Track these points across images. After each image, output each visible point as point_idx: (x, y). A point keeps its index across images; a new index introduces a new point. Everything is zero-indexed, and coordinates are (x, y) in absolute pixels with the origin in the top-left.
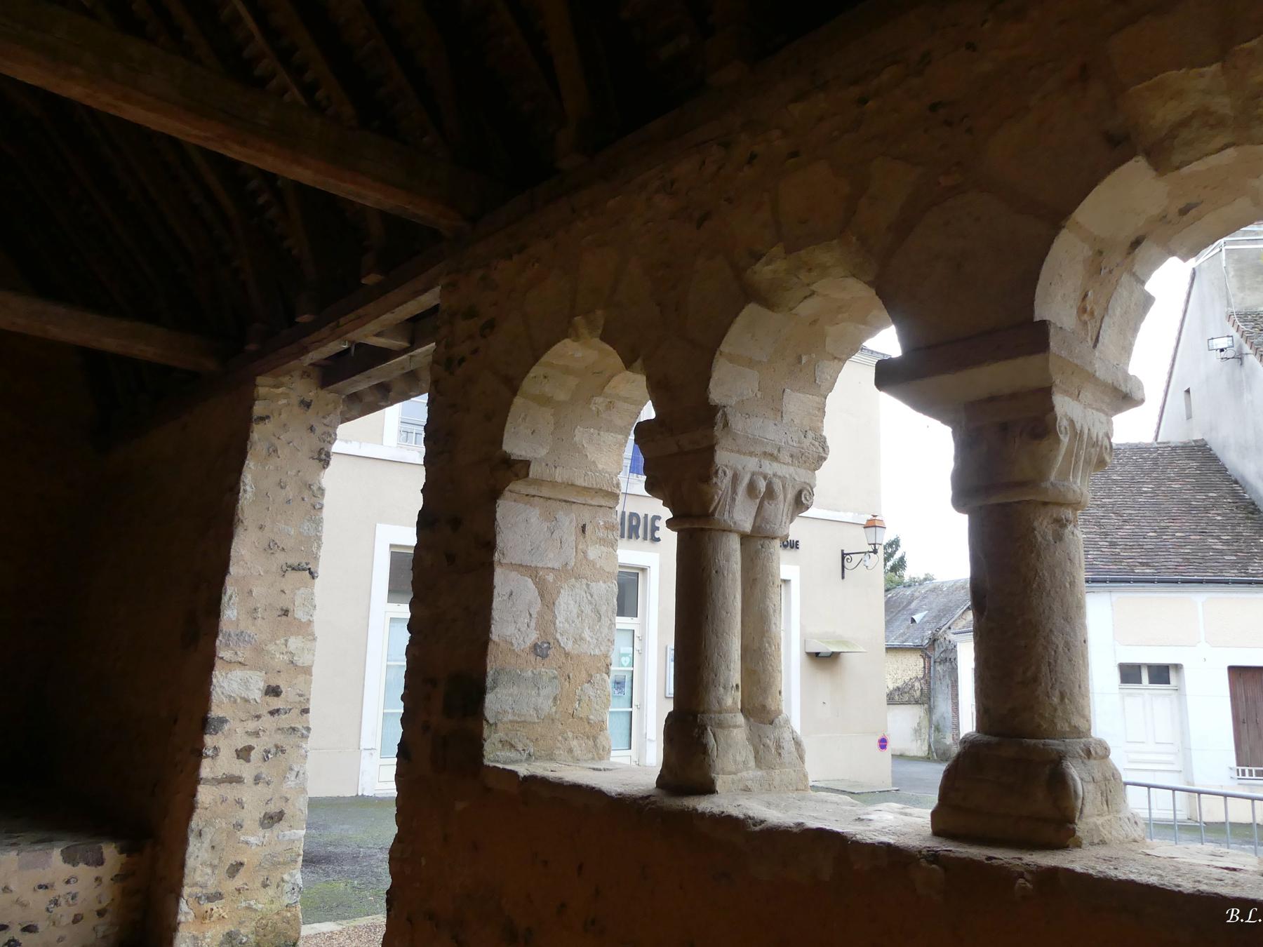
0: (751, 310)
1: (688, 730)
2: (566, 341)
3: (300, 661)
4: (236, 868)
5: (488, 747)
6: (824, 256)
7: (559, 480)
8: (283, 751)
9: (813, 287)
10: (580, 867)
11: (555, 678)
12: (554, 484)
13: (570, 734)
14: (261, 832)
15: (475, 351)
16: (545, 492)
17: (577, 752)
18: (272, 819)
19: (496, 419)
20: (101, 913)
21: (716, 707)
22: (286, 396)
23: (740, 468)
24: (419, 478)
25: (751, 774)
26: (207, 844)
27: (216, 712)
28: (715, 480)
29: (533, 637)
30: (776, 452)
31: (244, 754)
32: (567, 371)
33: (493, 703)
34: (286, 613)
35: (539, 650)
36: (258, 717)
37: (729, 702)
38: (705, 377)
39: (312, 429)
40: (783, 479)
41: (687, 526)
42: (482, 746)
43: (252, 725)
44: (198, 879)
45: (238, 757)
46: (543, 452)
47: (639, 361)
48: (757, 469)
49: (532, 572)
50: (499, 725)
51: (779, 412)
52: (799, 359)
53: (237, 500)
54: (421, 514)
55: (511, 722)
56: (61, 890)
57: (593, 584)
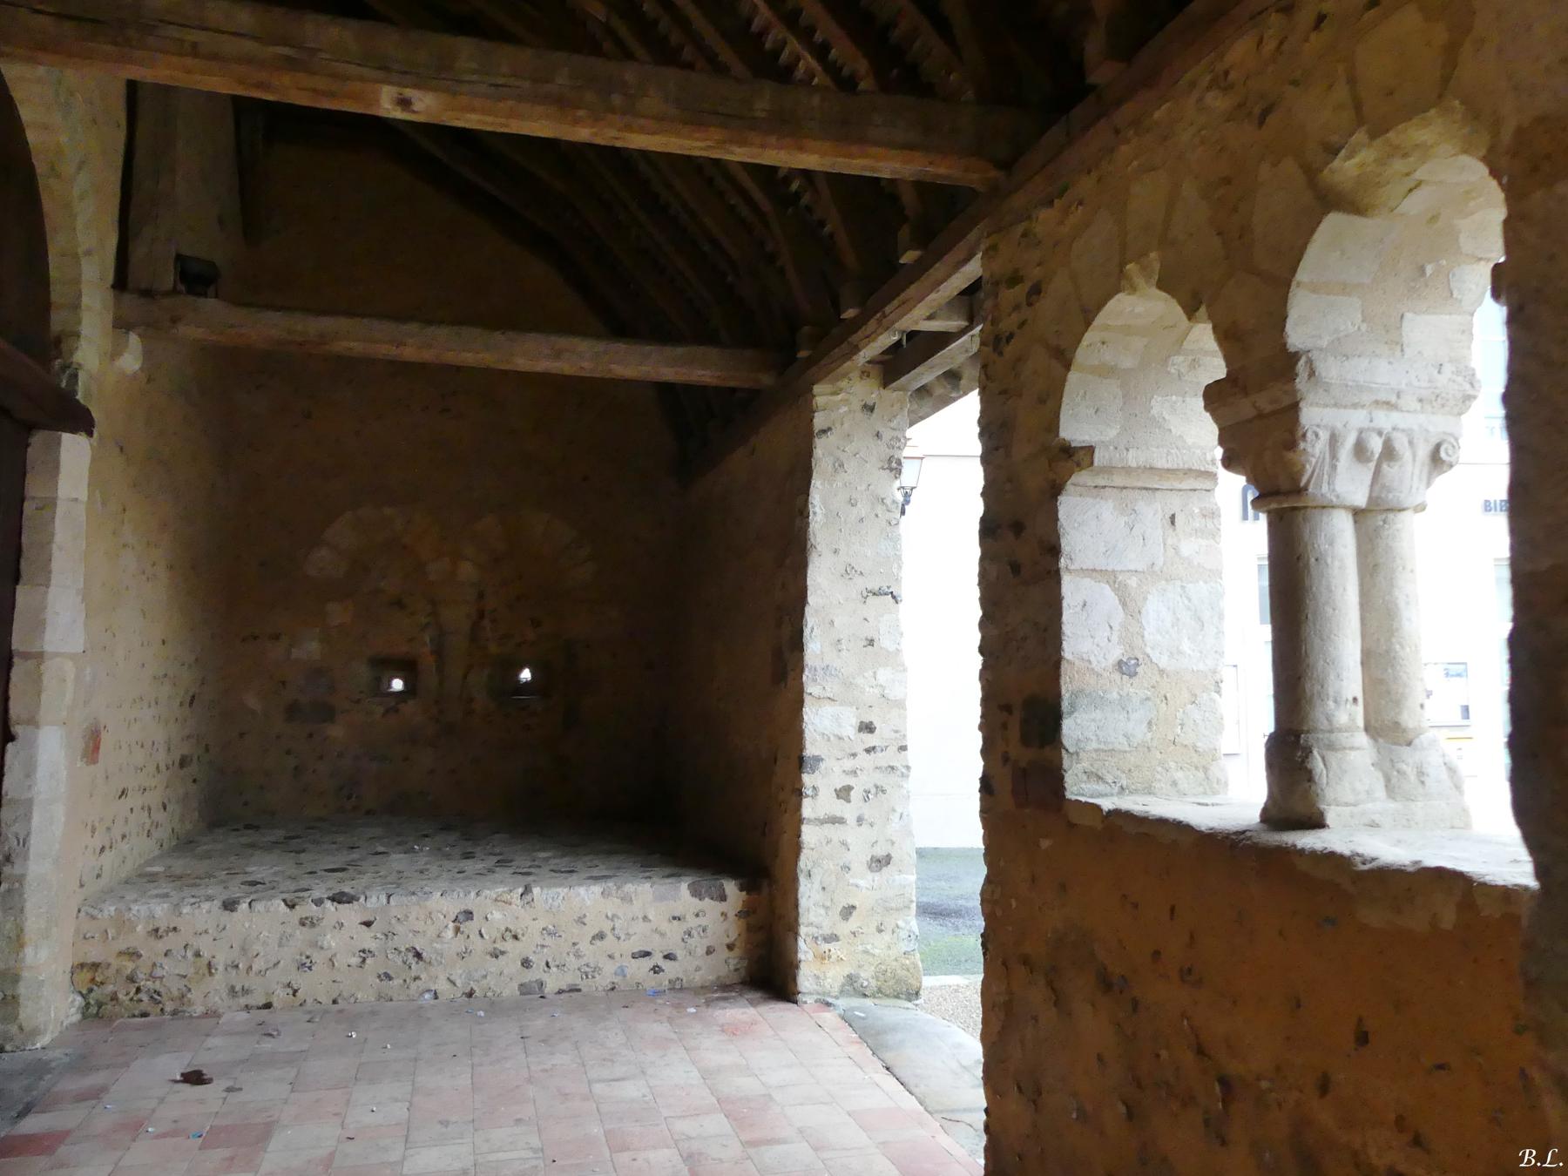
0: (1333, 222)
1: (1291, 753)
2: (1120, 296)
3: (893, 693)
4: (848, 911)
5: (1069, 780)
6: (1417, 133)
7: (1134, 465)
8: (883, 791)
9: (1418, 175)
10: (1172, 910)
11: (1148, 699)
12: (1128, 470)
13: (1172, 765)
14: (870, 876)
15: (1022, 324)
16: (1118, 481)
17: (1183, 785)
18: (881, 862)
19: (1050, 400)
20: (730, 947)
21: (1324, 724)
22: (846, 402)
23: (1339, 425)
24: (975, 477)
25: (1379, 804)
26: (817, 886)
27: (810, 750)
28: (1302, 445)
29: (1116, 653)
30: (1393, 399)
31: (844, 793)
32: (1128, 330)
33: (1071, 729)
34: (871, 642)
35: (1125, 668)
36: (854, 755)
37: (1342, 718)
38: (1279, 318)
39: (878, 435)
40: (1409, 433)
41: (1274, 506)
42: (1062, 778)
43: (849, 764)
44: (812, 918)
45: (838, 797)
46: (1112, 433)
47: (1203, 309)
48: (1366, 424)
49: (1108, 576)
50: (1082, 754)
51: (1397, 344)
52: (1422, 270)
53: (808, 524)
54: (983, 520)
55: (1096, 750)
56: (692, 922)
57: (1190, 586)
